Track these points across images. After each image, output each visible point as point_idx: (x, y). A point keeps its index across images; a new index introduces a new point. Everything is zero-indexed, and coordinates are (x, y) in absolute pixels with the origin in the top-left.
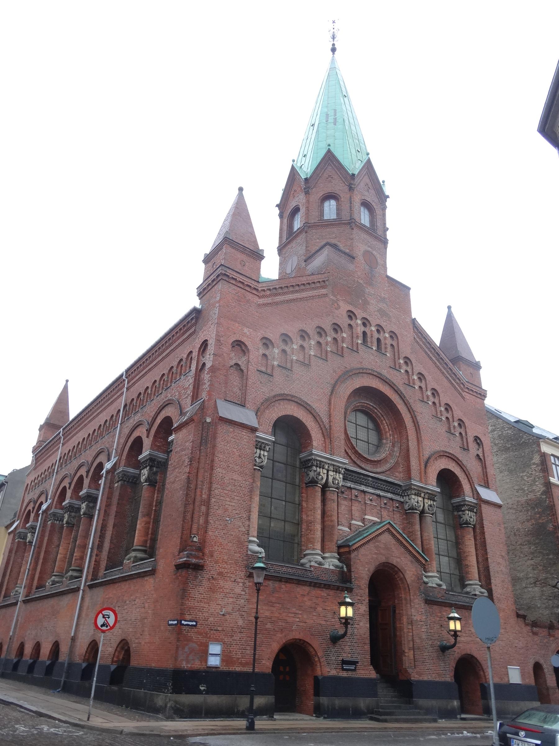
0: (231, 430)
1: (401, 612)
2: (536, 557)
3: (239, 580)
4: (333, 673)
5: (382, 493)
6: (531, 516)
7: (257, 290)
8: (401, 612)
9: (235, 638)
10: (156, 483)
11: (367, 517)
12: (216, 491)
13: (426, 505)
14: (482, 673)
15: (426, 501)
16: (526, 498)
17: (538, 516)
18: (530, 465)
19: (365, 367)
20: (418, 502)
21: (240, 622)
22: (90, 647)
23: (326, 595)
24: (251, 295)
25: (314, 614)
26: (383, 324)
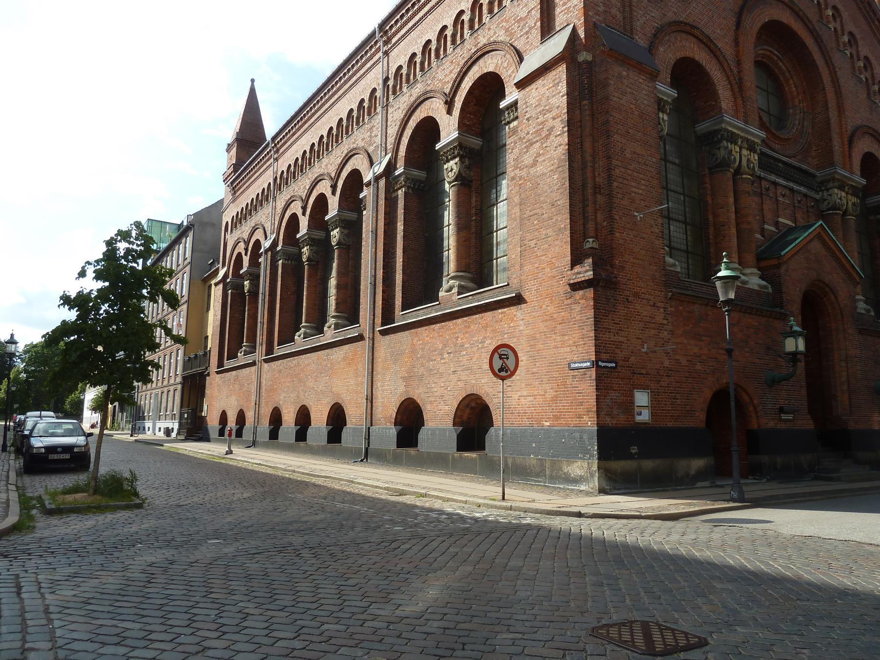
0: (625, 73)
3: (659, 304)
4: (771, 424)
5: (796, 187)
9: (662, 383)
10: (471, 181)
11: (781, 220)
12: (617, 171)
13: (850, 204)
15: (850, 197)
20: (841, 199)
21: (667, 363)
25: (747, 349)
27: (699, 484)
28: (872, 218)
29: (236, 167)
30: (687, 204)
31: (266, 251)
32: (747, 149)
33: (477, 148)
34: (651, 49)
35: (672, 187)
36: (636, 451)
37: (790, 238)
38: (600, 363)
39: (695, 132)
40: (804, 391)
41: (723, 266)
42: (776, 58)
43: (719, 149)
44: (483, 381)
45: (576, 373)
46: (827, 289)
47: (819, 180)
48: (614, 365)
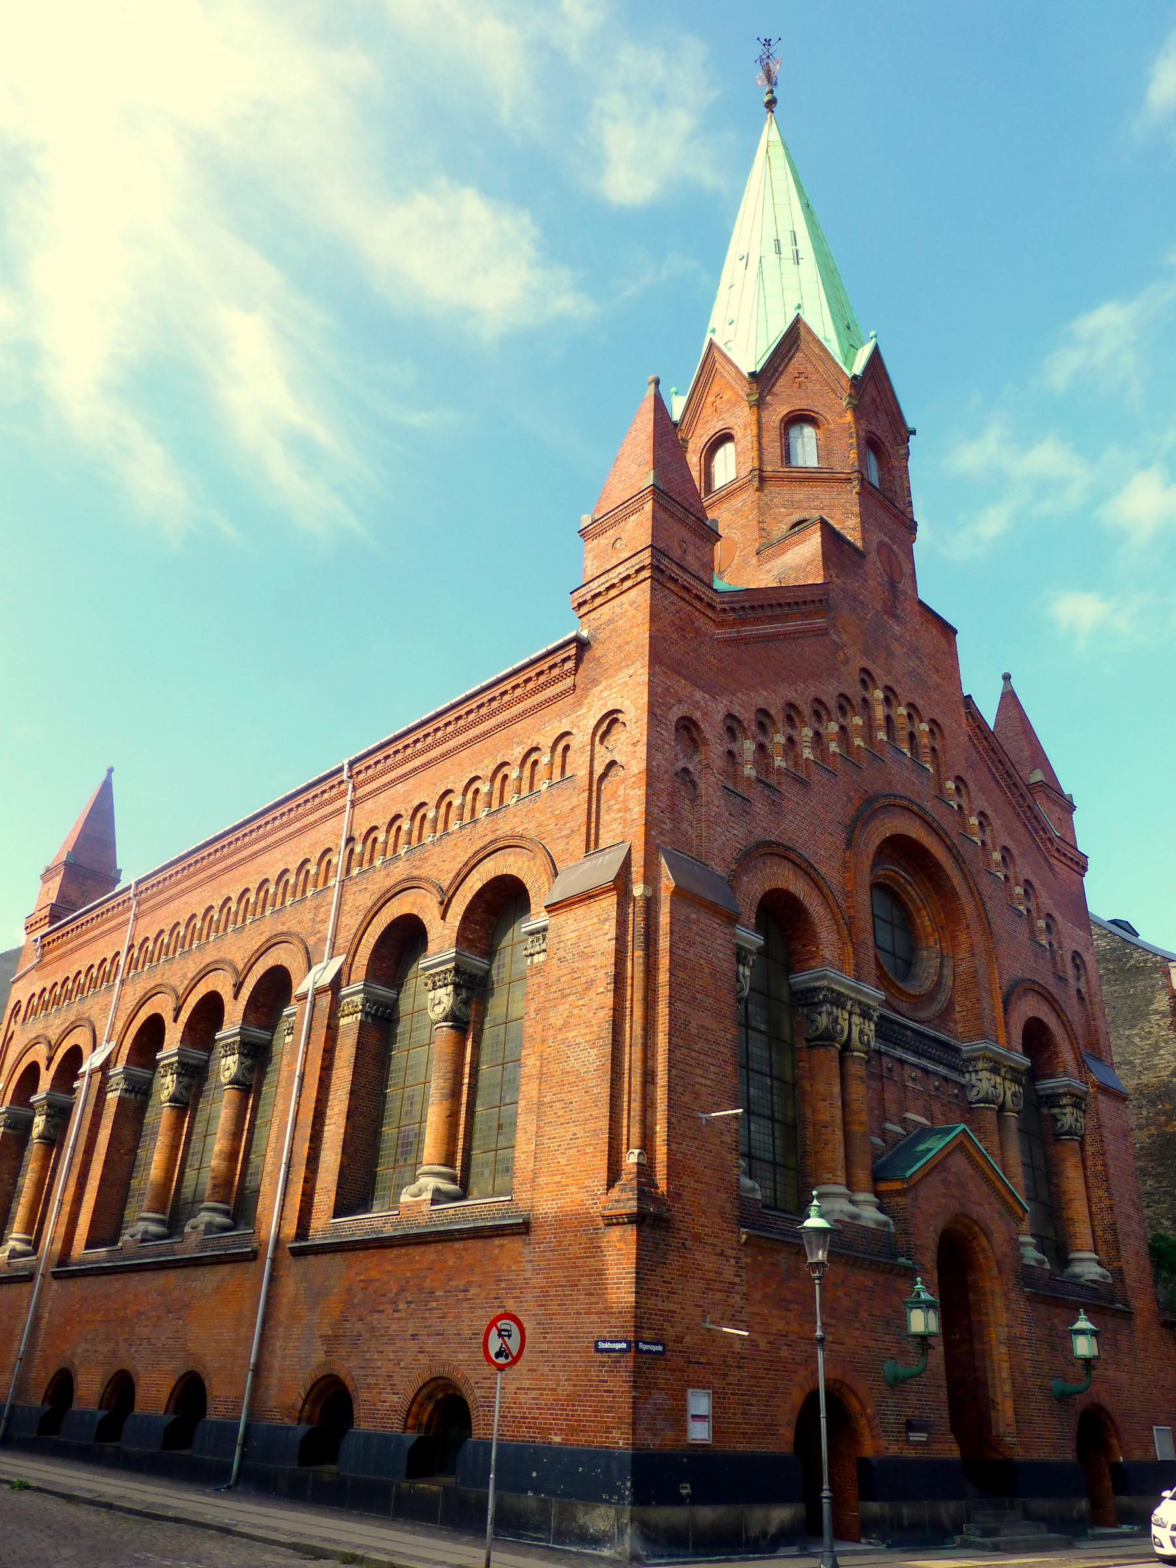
0: (694, 916)
1: (984, 1318)
2: (1158, 1202)
4: (894, 1450)
5: (931, 1066)
6: (1147, 1118)
7: (713, 608)
8: (984, 1318)
9: (731, 1379)
13: (1009, 1094)
14: (1114, 1441)
15: (1008, 1084)
16: (1136, 1082)
17: (1163, 1118)
18: (1148, 1014)
19: (895, 792)
20: (995, 1087)
22: (316, 1389)
23: (871, 1284)
24: (703, 619)
25: (856, 1325)
26: (919, 703)
27: (782, 1551)
28: (1045, 1111)
29: (56, 913)
30: (775, 1091)
31: (93, 1072)
32: (860, 1015)
33: (481, 973)
34: (733, 882)
35: (756, 1066)
36: (689, 1491)
37: (922, 1147)
38: (641, 1345)
39: (790, 986)
40: (943, 1394)
41: (813, 1212)
42: (902, 880)
43: (820, 1014)
44: (460, 1357)
45: (604, 1358)
46: (977, 1228)
47: (965, 1056)
48: (660, 1348)
